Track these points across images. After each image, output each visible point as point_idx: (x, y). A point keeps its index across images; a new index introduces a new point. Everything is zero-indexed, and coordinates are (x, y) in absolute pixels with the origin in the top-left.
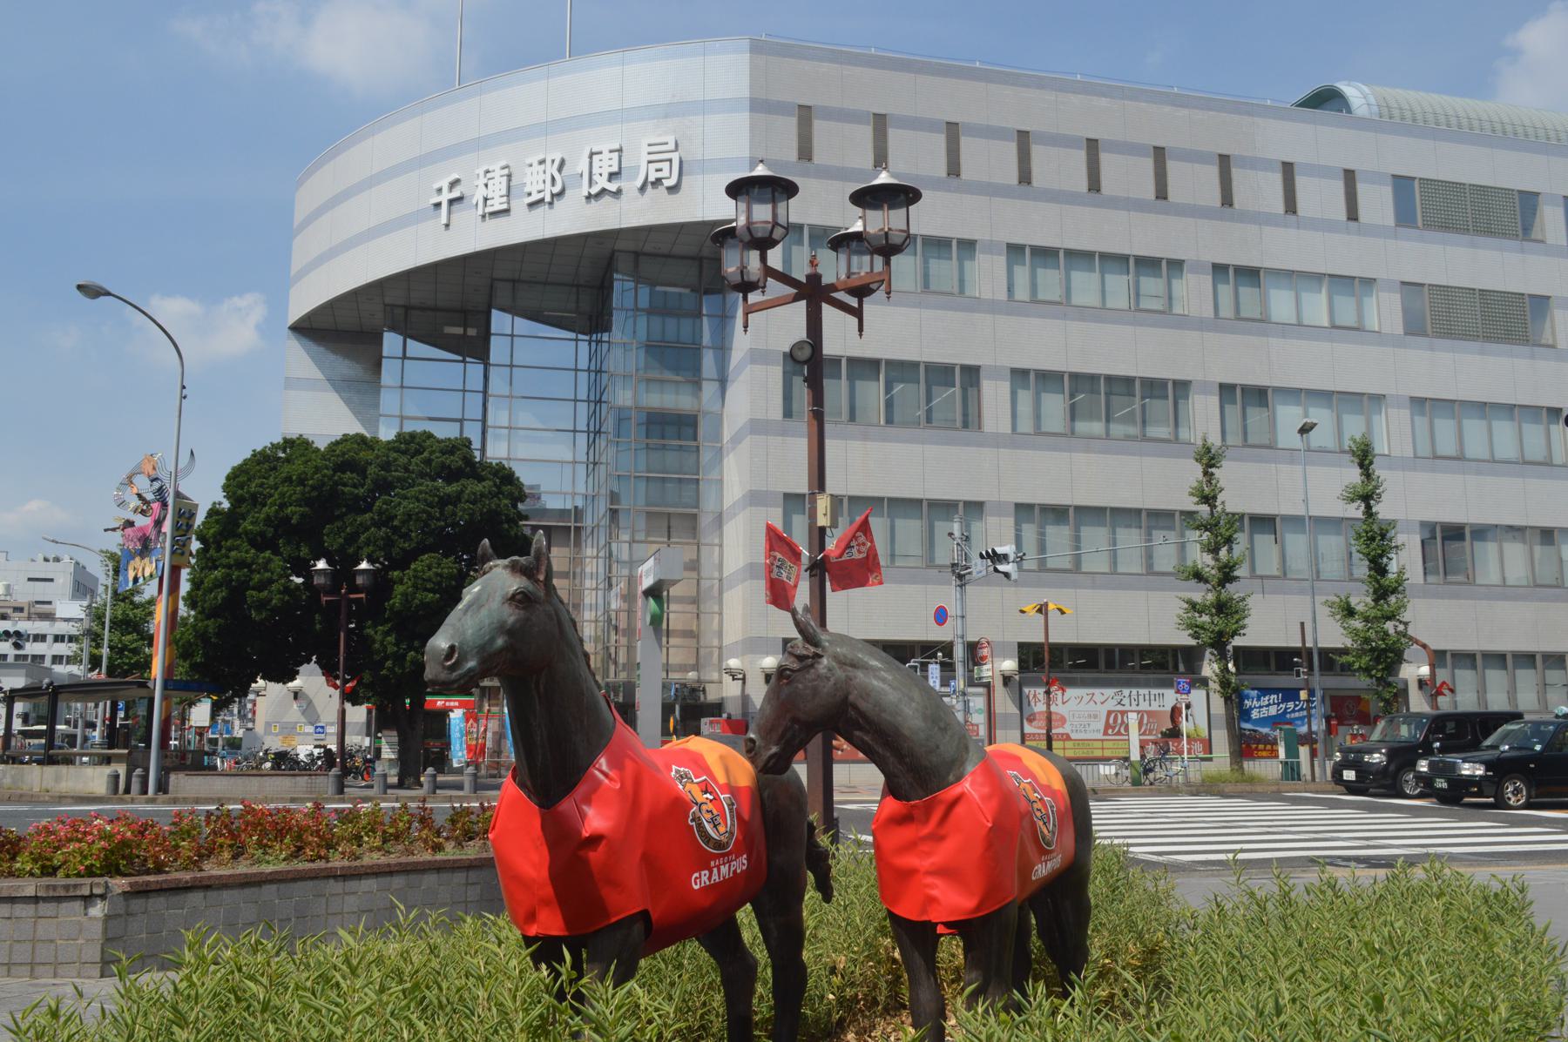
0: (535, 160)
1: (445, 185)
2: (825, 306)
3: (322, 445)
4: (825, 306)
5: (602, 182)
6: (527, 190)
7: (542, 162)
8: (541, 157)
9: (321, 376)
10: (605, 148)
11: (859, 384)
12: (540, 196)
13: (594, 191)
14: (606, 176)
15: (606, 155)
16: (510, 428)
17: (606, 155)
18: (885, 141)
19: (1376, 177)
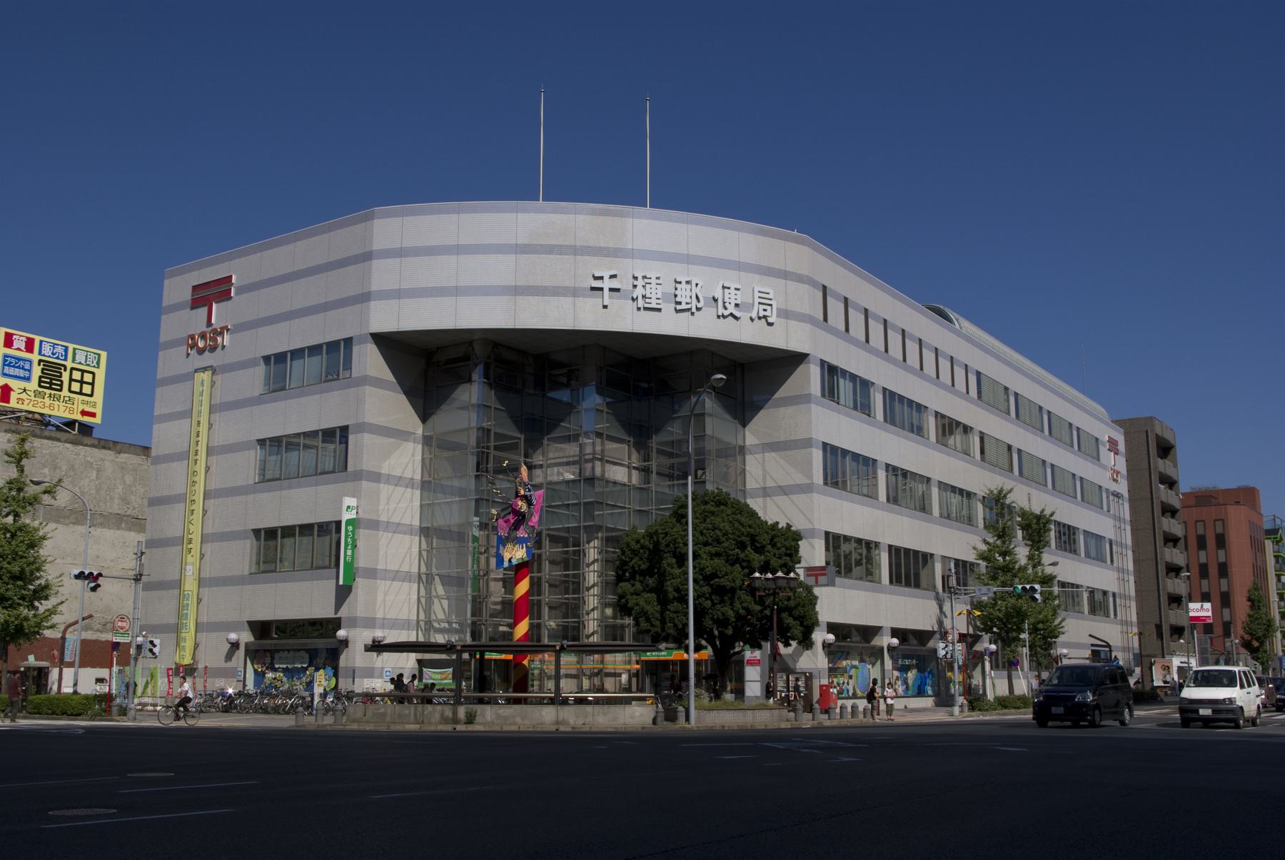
5: (731, 309)
7: (688, 282)
13: (726, 313)
19: (877, 318)
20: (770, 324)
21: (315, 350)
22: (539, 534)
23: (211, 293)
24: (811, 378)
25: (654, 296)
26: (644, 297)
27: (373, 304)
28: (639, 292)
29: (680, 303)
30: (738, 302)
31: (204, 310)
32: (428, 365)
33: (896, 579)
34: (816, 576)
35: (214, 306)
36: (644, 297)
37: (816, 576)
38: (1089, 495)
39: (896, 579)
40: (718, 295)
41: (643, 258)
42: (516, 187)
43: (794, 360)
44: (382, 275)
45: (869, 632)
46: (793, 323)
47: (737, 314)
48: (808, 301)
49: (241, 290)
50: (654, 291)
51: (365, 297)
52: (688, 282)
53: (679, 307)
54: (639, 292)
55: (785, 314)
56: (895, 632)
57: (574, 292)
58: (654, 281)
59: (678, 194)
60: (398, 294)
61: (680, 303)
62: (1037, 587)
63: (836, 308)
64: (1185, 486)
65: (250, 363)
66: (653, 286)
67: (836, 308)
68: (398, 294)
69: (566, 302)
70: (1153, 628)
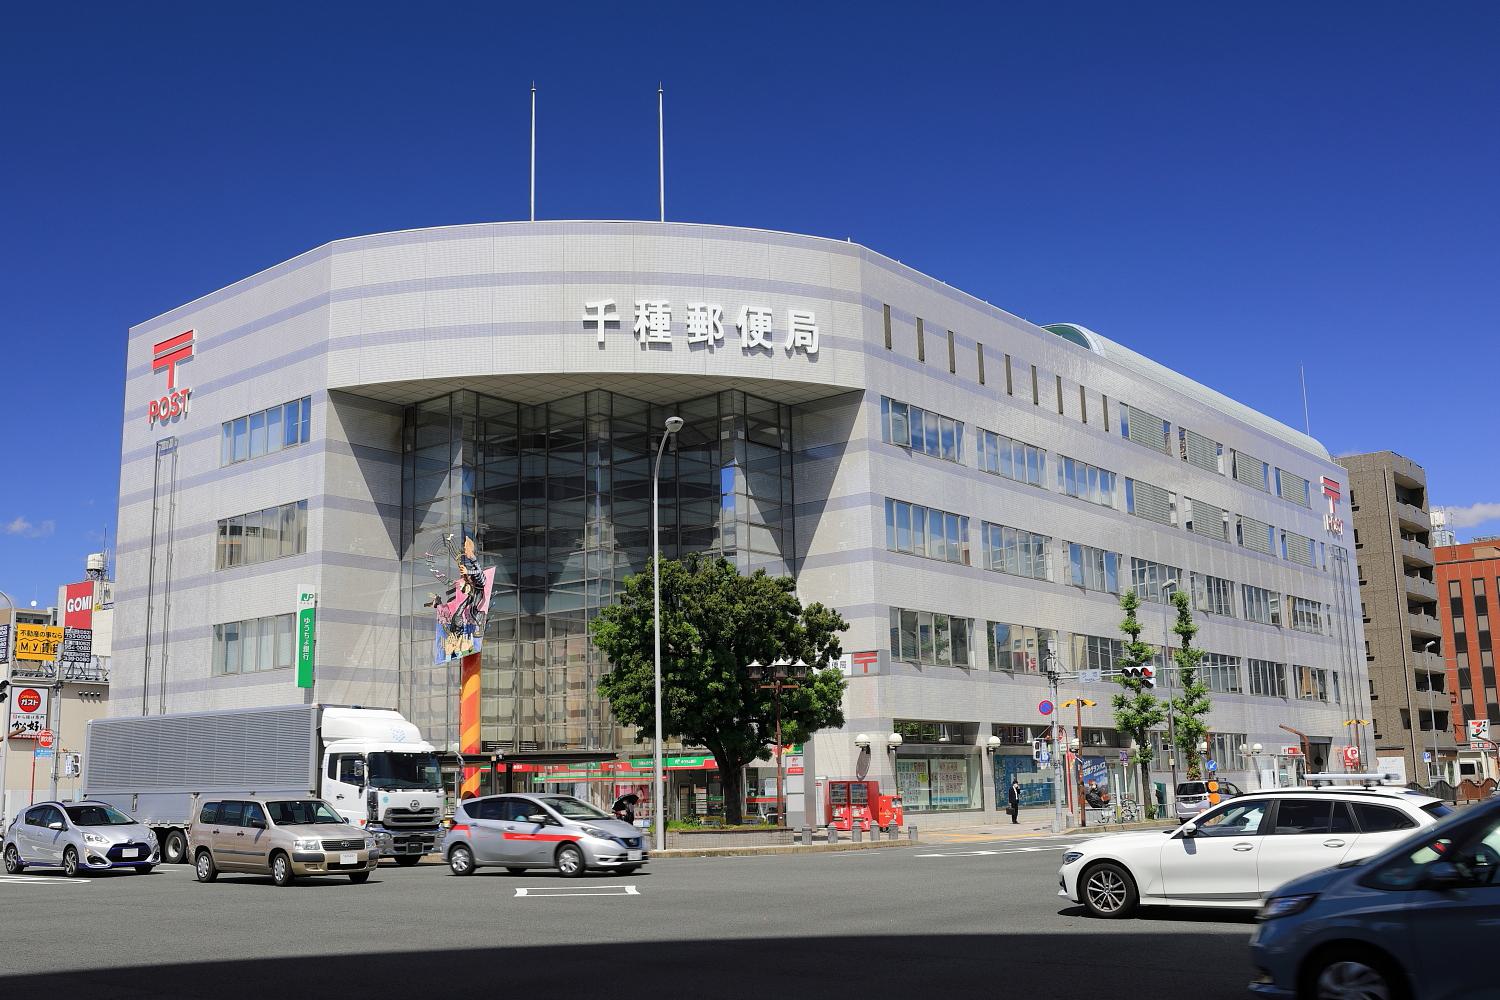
0: (697, 306)
1: (601, 305)
2: (168, 371)
3: (1256, 810)
4: (168, 371)
5: (759, 339)
6: (690, 330)
7: (703, 309)
8: (703, 305)
9: (369, 498)
10: (761, 310)
11: (230, 642)
12: (704, 338)
13: (753, 344)
14: (761, 334)
15: (761, 317)
16: (148, 641)
17: (761, 317)
18: (923, 340)
19: (967, 342)
20: (813, 357)
21: (272, 413)
22: (1104, 678)
23: (172, 354)
24: (866, 422)
25: (660, 328)
26: (648, 330)
27: (330, 354)
28: (642, 324)
29: (693, 335)
30: (769, 330)
31: (166, 373)
32: (403, 432)
33: (1256, 688)
34: (866, 662)
35: (177, 369)
36: (648, 330)
37: (866, 662)
38: (1296, 549)
39: (1256, 688)
40: (741, 321)
41: (646, 282)
42: (506, 207)
43: (853, 396)
44: (340, 319)
45: (964, 732)
46: (841, 352)
47: (768, 344)
48: (854, 322)
49: (202, 348)
50: (660, 322)
51: (322, 348)
52: (703, 309)
53: (692, 340)
54: (642, 324)
55: (829, 341)
56: (998, 729)
57: (563, 328)
58: (660, 309)
59: (703, 201)
60: (358, 342)
61: (693, 335)
62: (1150, 668)
63: (904, 334)
64: (1438, 540)
65: (205, 434)
66: (660, 315)
67: (904, 334)
68: (358, 342)
69: (553, 339)
70: (1398, 715)
